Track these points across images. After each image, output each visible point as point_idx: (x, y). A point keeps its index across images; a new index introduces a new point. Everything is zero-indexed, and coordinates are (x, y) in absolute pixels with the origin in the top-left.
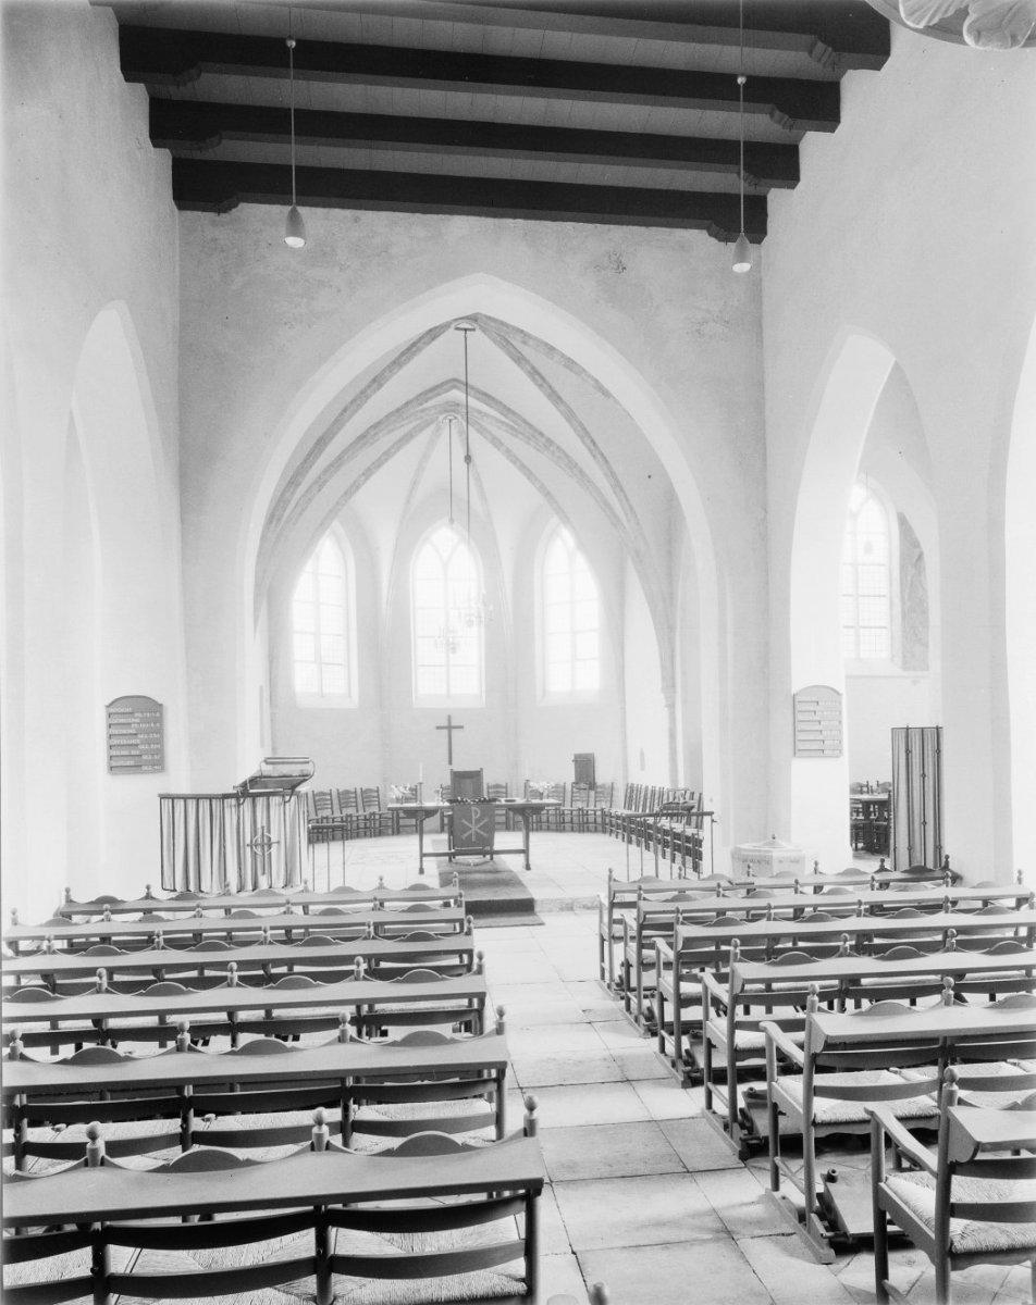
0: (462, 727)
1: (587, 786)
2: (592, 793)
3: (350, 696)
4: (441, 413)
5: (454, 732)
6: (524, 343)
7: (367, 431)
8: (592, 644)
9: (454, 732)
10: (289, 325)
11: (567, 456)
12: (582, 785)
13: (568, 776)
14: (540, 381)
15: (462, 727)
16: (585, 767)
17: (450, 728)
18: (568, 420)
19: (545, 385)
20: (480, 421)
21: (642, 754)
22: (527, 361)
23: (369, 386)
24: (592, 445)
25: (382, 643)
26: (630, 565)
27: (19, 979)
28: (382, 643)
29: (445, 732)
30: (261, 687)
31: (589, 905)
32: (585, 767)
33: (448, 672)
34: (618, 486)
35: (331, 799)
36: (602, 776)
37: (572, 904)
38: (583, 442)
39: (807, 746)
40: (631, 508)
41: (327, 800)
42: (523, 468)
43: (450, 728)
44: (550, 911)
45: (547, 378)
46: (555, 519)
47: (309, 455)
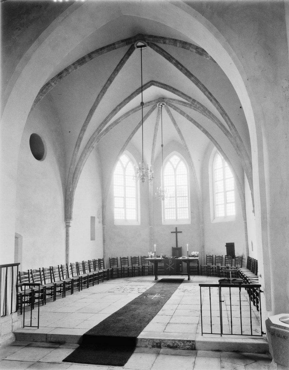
0: (181, 232)
1: (231, 257)
2: (234, 260)
3: (138, 221)
4: (157, 103)
5: (178, 234)
6: (164, 43)
7: (116, 108)
8: (232, 196)
9: (178, 234)
10: (18, 29)
11: (202, 106)
12: (229, 256)
13: (223, 252)
14: (181, 67)
15: (181, 232)
16: (230, 247)
17: (176, 232)
18: (196, 84)
19: (183, 68)
20: (173, 104)
21: (252, 243)
22: (174, 59)
23: (107, 83)
24: (210, 95)
25: (151, 202)
26: (169, 107)
27: (189, 279)
28: (151, 202)
29: (175, 234)
30: (93, 219)
31: (171, 345)
32: (230, 247)
33: (176, 211)
34: (224, 113)
35: (128, 261)
36: (238, 252)
37: (160, 343)
38: (205, 94)
39: (26, 280)
40: (232, 124)
41: (126, 261)
42: (195, 123)
43: (176, 232)
44: (146, 347)
45: (213, 95)
46: (215, 149)
47: (87, 117)
